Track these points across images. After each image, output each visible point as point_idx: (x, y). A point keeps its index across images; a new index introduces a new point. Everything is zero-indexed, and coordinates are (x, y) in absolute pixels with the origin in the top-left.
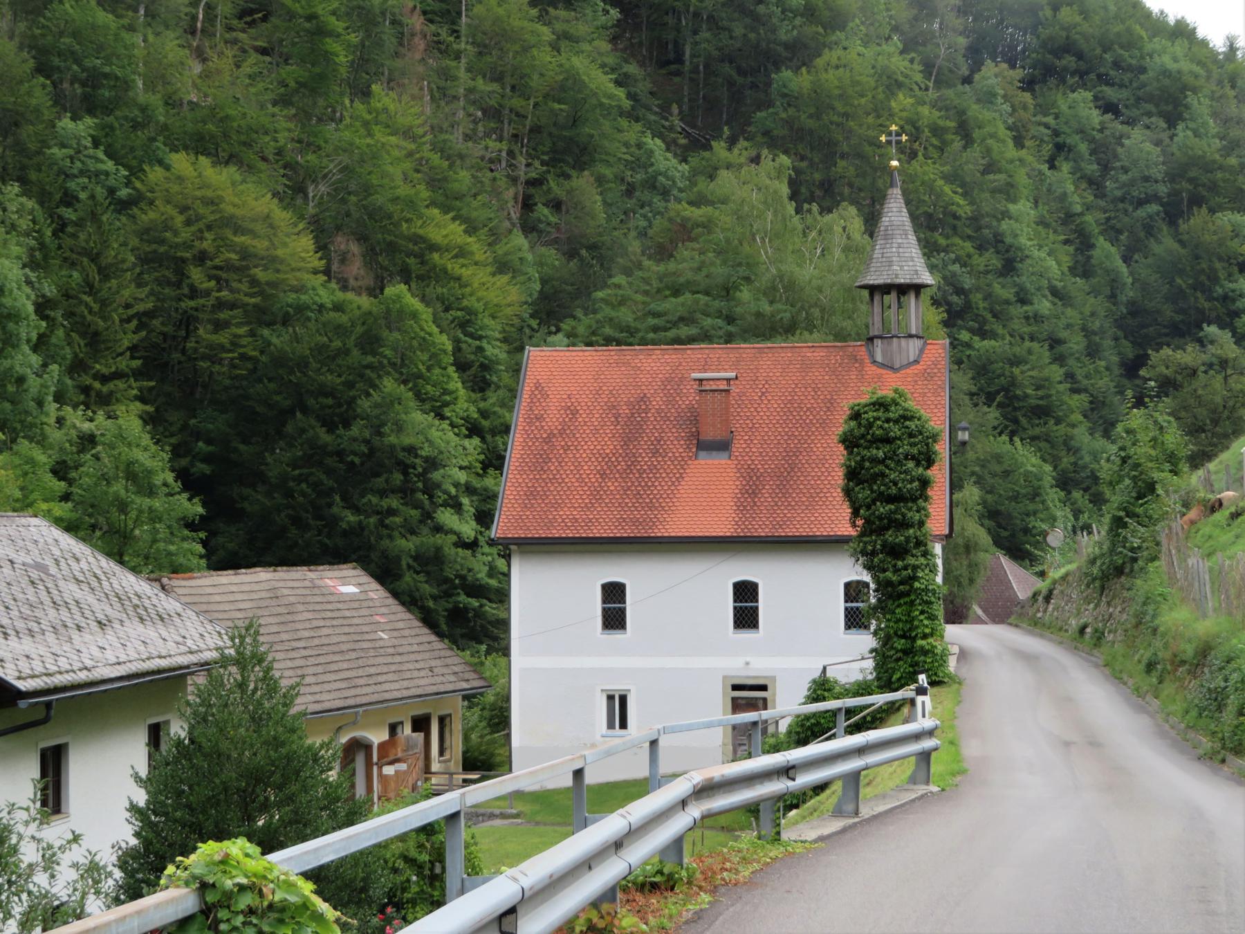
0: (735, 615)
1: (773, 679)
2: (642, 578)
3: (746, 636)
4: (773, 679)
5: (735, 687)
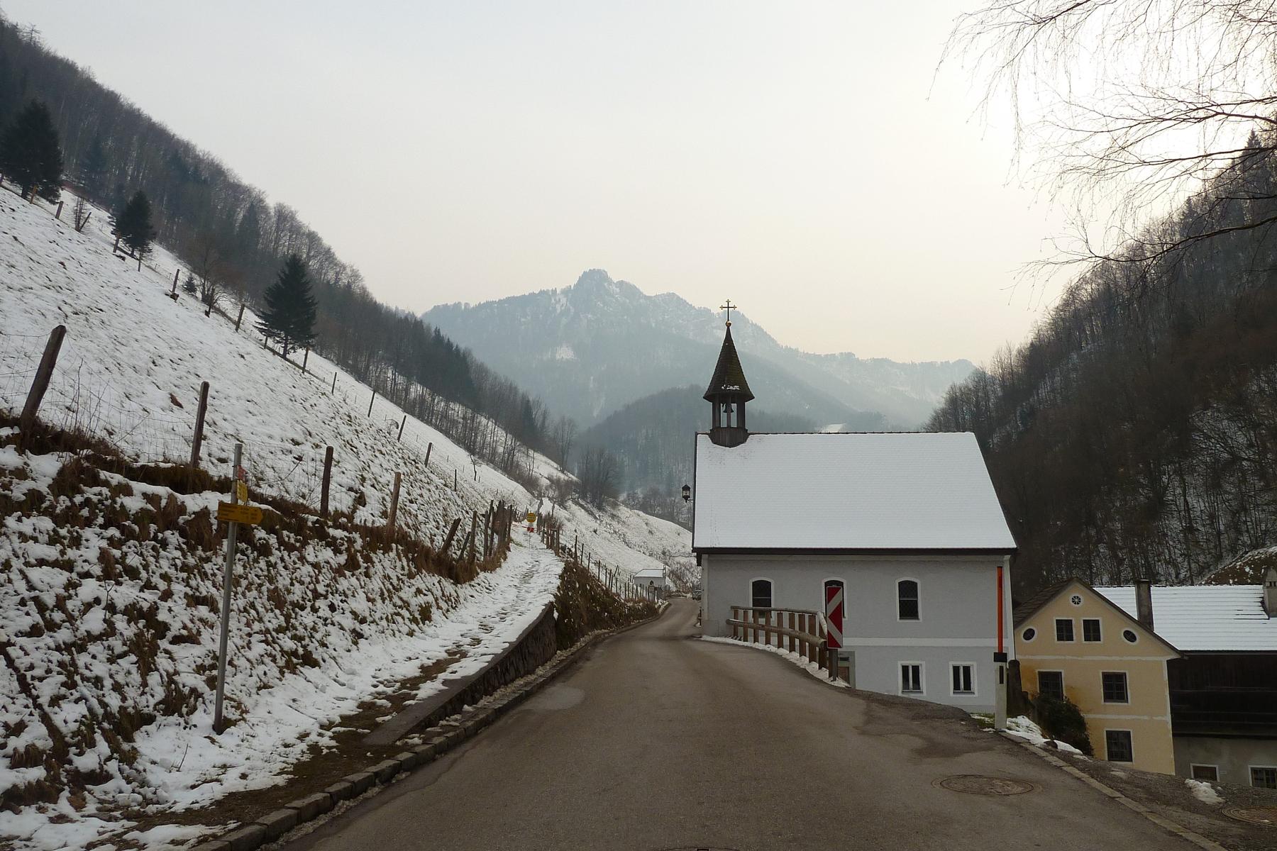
1: (852, 653)
4: (852, 653)
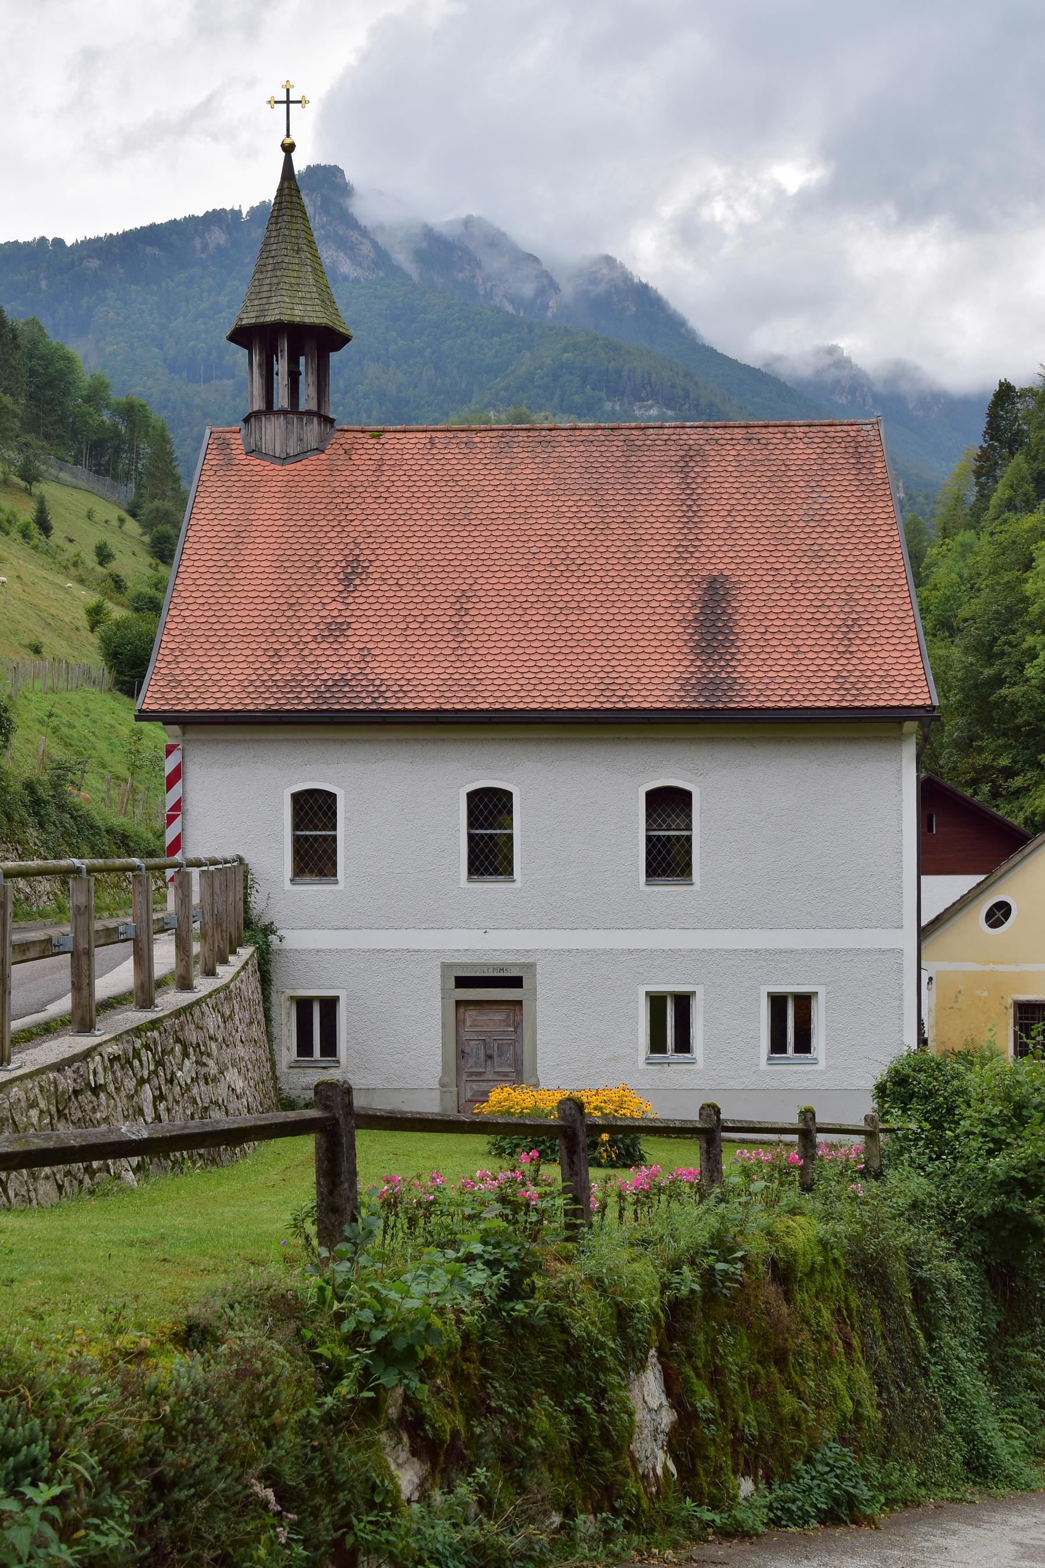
0: (648, 852)
1: (531, 967)
2: (731, 794)
3: (491, 888)
4: (531, 967)
5: (462, 982)
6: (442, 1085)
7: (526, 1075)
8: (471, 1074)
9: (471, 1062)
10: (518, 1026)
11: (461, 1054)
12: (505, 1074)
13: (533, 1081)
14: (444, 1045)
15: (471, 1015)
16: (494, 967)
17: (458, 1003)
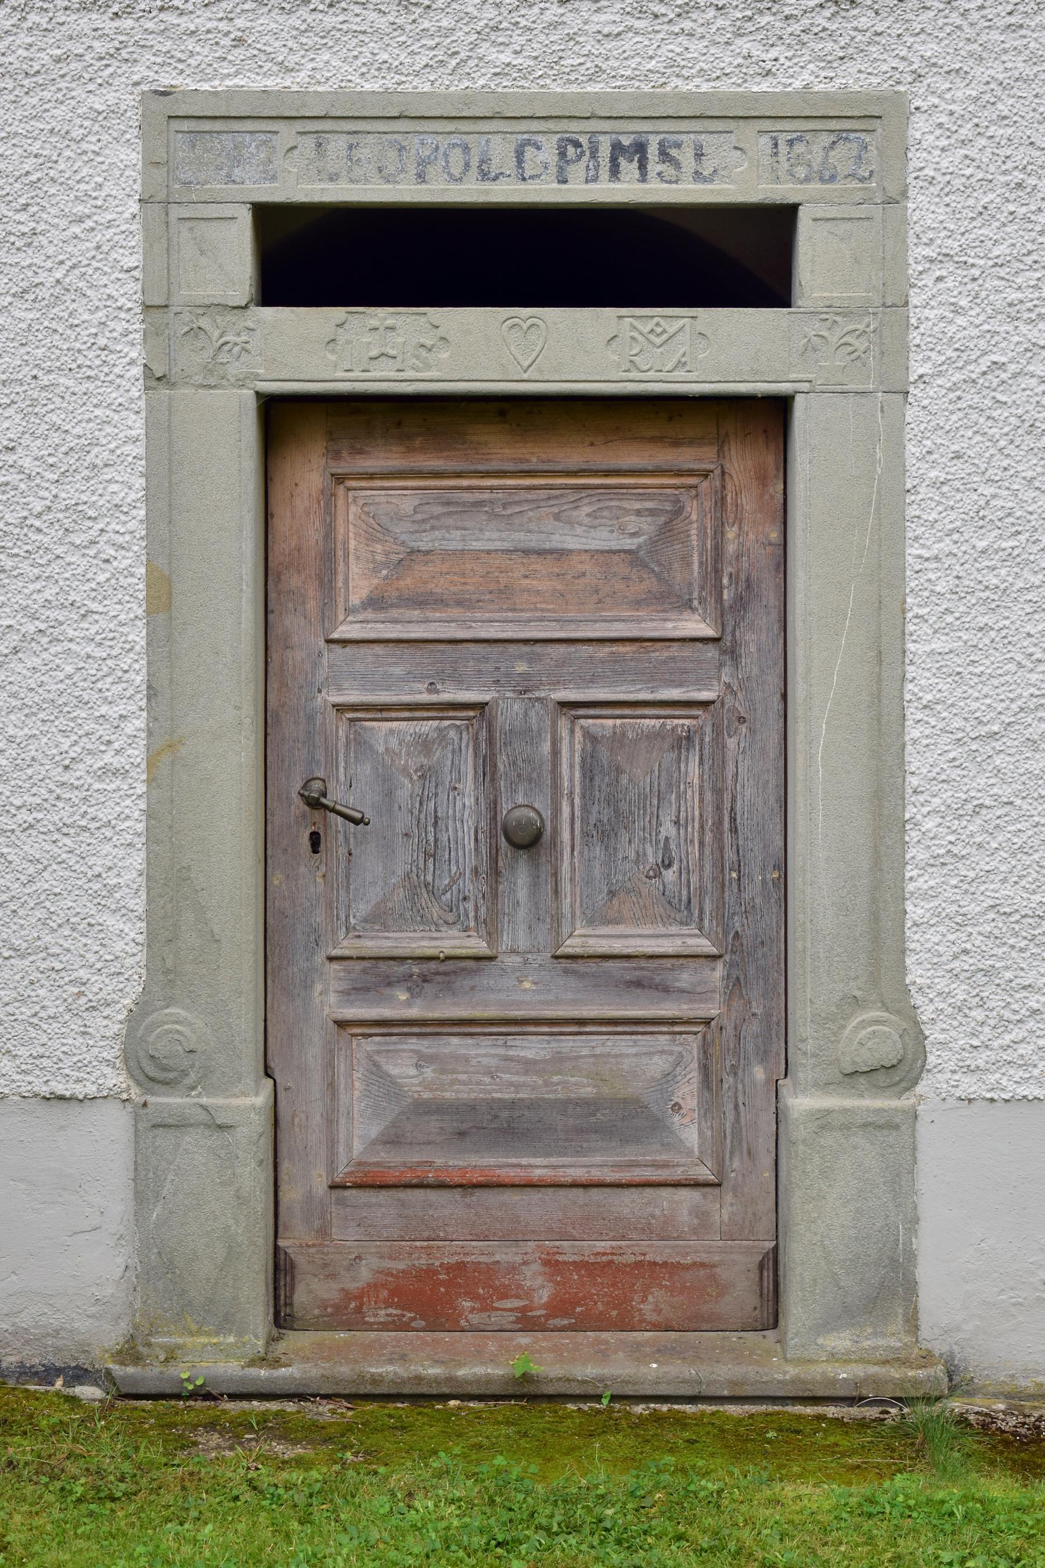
5: (317, 256)
6: (152, 1068)
7: (817, 982)
8: (378, 972)
9: (377, 873)
10: (753, 598)
11: (303, 820)
12: (644, 973)
13: (869, 1036)
14: (166, 753)
15: (378, 518)
16: (573, 131)
17: (282, 418)
